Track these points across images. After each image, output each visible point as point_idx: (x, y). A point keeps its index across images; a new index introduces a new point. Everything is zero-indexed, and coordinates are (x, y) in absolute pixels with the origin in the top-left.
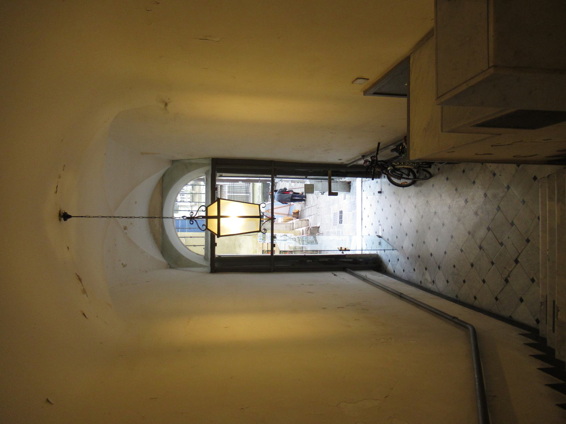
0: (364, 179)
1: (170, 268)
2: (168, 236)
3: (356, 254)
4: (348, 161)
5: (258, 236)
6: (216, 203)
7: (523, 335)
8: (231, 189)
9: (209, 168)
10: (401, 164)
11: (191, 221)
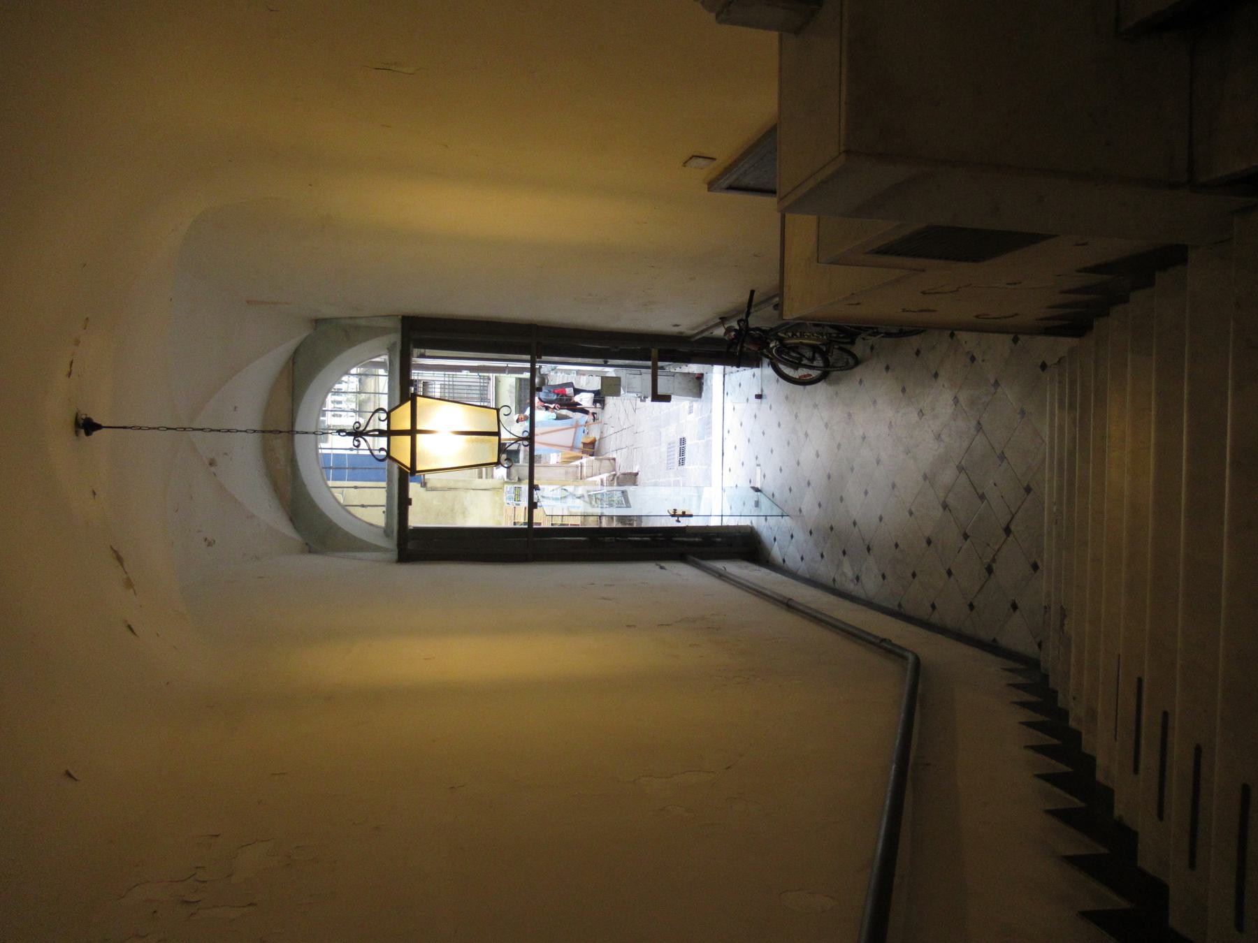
0: (728, 368)
1: (311, 551)
2: (306, 483)
3: (707, 526)
4: (693, 329)
5: (505, 490)
6: (408, 404)
7: (1011, 670)
8: (447, 391)
9: (396, 338)
10: (797, 336)
11: (357, 440)
